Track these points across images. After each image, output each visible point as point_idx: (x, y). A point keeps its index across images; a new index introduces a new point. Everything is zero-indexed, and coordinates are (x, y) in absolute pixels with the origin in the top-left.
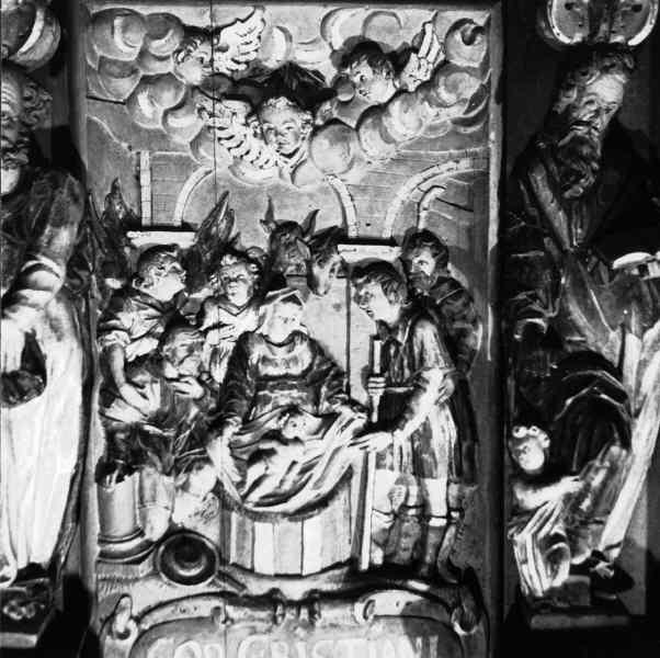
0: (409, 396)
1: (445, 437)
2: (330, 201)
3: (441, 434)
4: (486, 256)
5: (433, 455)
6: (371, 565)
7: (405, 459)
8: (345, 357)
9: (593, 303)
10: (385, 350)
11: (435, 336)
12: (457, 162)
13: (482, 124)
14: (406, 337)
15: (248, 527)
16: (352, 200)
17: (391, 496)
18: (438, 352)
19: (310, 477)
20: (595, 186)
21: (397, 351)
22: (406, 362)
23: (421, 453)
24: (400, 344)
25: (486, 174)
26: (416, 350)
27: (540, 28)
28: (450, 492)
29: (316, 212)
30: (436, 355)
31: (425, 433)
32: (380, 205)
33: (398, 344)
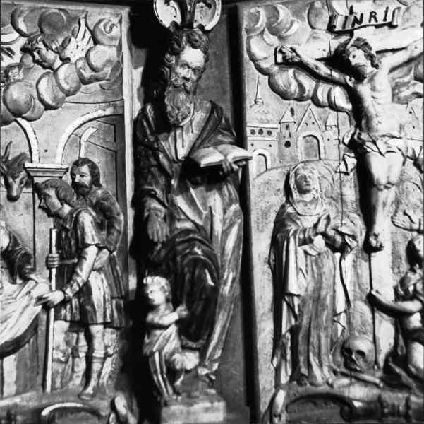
0: (75, 265)
1: (100, 293)
2: (20, 135)
3: (99, 291)
4: (127, 244)
5: (93, 306)
6: (65, 308)
7: (74, 311)
8: (32, 243)
9: (191, 195)
10: (59, 235)
11: (92, 223)
12: (104, 110)
13: (119, 84)
14: (72, 226)
15: (113, 43)
16: (35, 134)
17: (83, 217)
18: (94, 233)
19: (7, 325)
20: (395, 412)
21: (66, 236)
22: (73, 242)
23: (85, 305)
24: (69, 230)
25: (122, 116)
26: (79, 233)
27: (250, 8)
28: (100, 366)
29: (10, 143)
30: (92, 236)
31: (85, 291)
32: (54, 139)
33: (67, 230)
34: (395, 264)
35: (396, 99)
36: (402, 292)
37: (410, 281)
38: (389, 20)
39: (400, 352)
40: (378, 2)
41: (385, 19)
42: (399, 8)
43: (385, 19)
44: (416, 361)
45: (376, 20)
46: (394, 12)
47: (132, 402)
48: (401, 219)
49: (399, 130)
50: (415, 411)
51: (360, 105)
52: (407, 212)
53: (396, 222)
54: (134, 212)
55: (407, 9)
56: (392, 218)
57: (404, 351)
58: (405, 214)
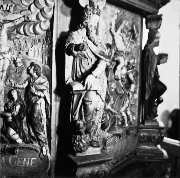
34: (4, 99)
35: (9, 39)
36: (6, 109)
37: (9, 105)
38: (8, 9)
39: (4, 130)
40: (5, 1)
41: (6, 9)
42: (12, 5)
43: (6, 9)
44: (89, 94)
45: (3, 9)
46: (10, 6)
47: (56, 96)
48: (8, 83)
49: (8, 51)
50: (7, 150)
51: (152, 21)
52: (10, 80)
53: (7, 83)
54: (78, 44)
55: (15, 6)
56: (5, 82)
57: (6, 129)
58: (10, 81)
